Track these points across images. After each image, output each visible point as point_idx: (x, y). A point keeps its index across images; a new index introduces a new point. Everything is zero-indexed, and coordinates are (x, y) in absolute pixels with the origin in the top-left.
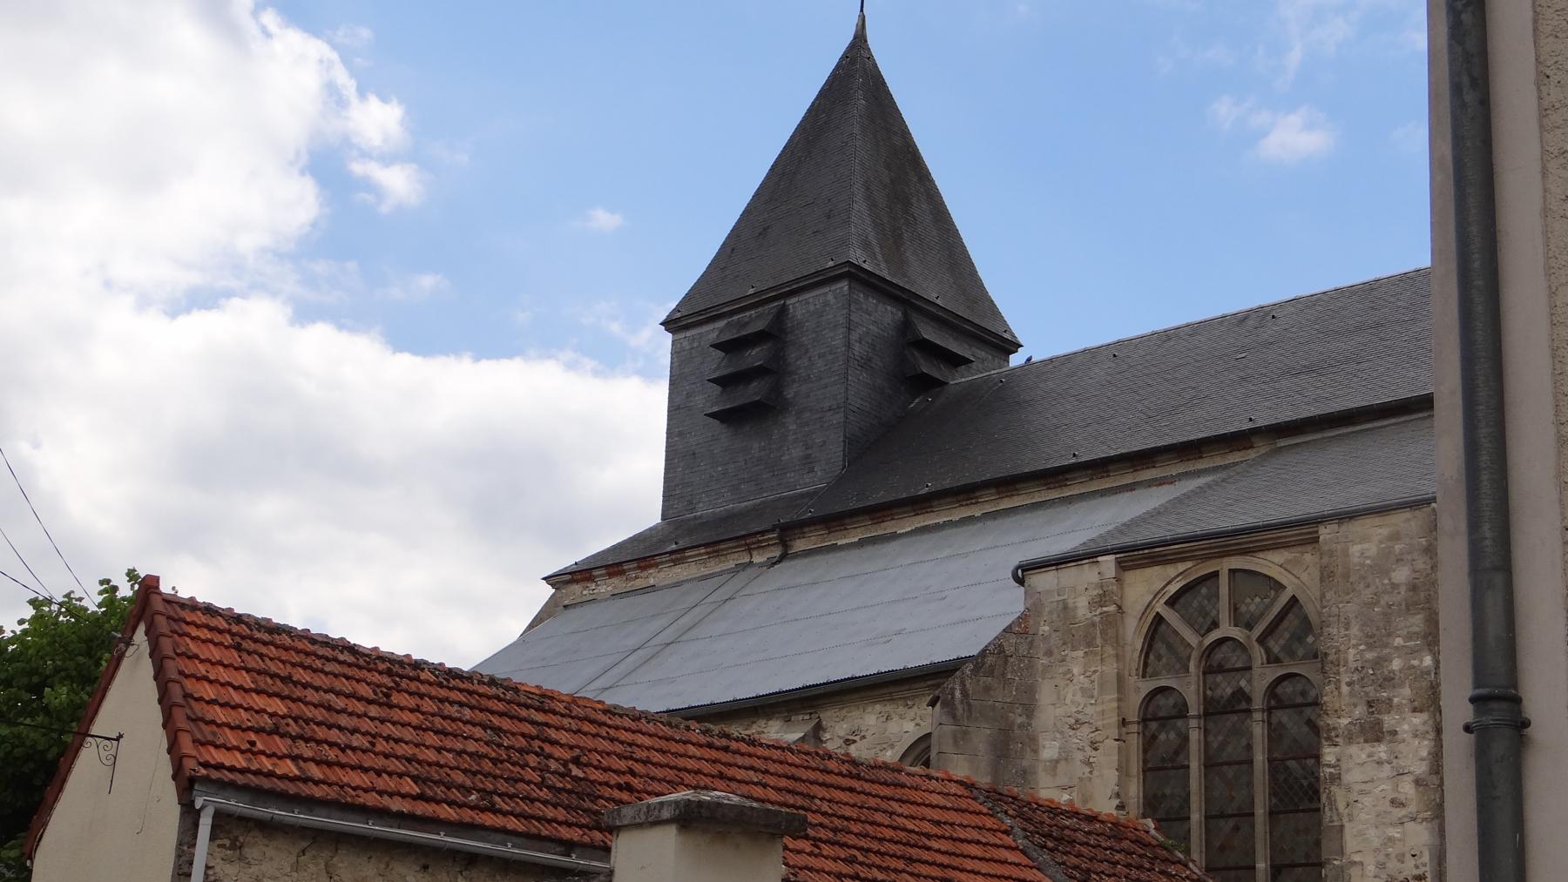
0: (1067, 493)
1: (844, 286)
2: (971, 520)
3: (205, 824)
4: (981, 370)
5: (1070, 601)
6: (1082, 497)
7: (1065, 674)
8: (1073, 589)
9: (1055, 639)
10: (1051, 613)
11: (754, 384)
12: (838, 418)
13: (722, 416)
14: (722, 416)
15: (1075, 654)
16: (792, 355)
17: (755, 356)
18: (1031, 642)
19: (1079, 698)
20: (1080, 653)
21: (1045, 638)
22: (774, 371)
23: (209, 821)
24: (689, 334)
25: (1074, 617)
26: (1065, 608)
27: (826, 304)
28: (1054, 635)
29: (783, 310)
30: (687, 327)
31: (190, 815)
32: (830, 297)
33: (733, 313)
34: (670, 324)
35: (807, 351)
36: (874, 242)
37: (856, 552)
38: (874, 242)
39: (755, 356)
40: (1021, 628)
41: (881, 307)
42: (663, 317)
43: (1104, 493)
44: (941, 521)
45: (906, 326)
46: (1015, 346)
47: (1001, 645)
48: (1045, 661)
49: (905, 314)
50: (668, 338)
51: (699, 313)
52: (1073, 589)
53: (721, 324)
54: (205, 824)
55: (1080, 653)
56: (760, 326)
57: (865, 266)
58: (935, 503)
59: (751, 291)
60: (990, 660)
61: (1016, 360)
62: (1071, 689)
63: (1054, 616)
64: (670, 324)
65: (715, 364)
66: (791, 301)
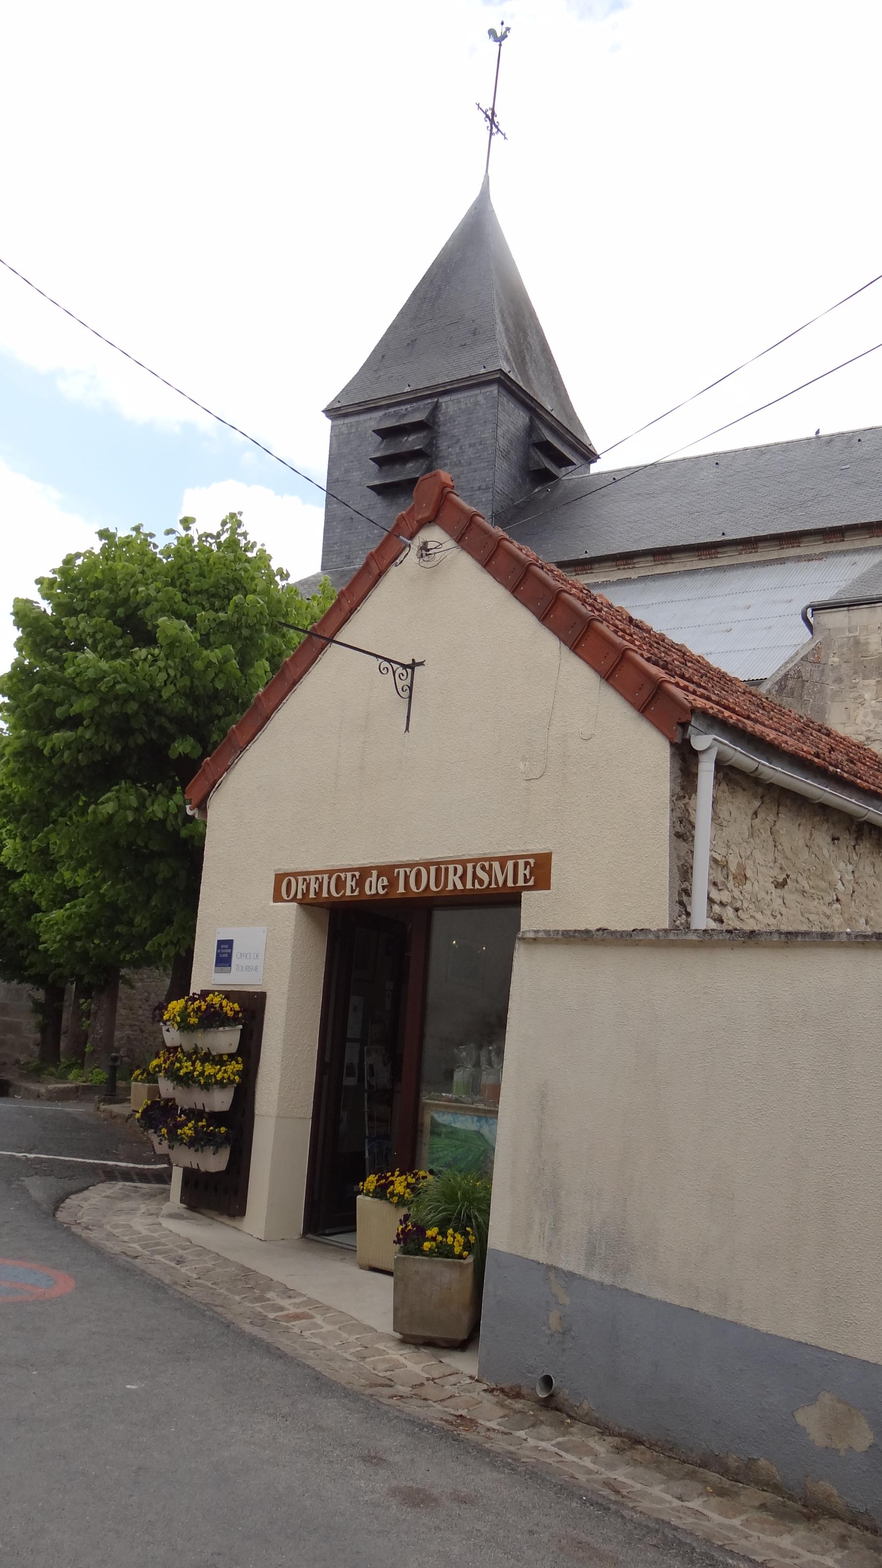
0: (716, 563)
1: (494, 389)
2: (628, 581)
3: (706, 771)
4: (568, 476)
5: (862, 639)
6: (732, 567)
7: (855, 699)
8: (866, 627)
9: (845, 669)
10: (841, 646)
11: (410, 465)
12: (488, 496)
13: (380, 490)
14: (380, 490)
15: (867, 682)
16: (443, 444)
17: (413, 442)
18: (823, 671)
19: (870, 719)
20: (873, 682)
21: (834, 668)
22: (426, 456)
23: (712, 766)
24: (347, 421)
25: (866, 651)
26: (857, 642)
27: (476, 403)
28: (844, 665)
29: (436, 407)
30: (345, 415)
31: (685, 758)
32: (480, 398)
33: (389, 406)
34: (332, 412)
35: (458, 441)
36: (511, 358)
37: (640, 586)
38: (511, 358)
39: (413, 442)
40: (813, 658)
41: (516, 411)
42: (324, 407)
43: (754, 565)
44: (600, 580)
45: (531, 429)
46: (590, 456)
47: (799, 671)
48: (834, 687)
49: (531, 420)
50: (328, 423)
51: (359, 404)
52: (866, 627)
53: (379, 414)
54: (706, 771)
55: (873, 682)
56: (419, 417)
57: (511, 375)
58: (596, 566)
59: (407, 389)
60: (791, 683)
61: (595, 468)
62: (862, 711)
63: (845, 650)
64: (332, 412)
65: (375, 448)
66: (443, 400)
